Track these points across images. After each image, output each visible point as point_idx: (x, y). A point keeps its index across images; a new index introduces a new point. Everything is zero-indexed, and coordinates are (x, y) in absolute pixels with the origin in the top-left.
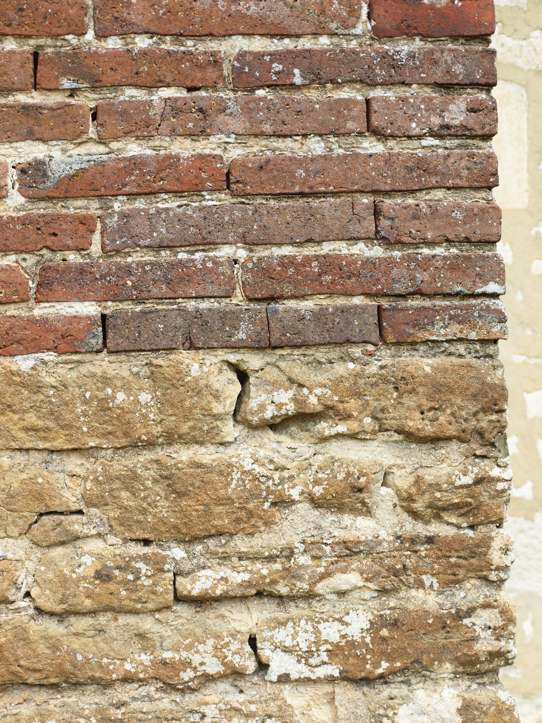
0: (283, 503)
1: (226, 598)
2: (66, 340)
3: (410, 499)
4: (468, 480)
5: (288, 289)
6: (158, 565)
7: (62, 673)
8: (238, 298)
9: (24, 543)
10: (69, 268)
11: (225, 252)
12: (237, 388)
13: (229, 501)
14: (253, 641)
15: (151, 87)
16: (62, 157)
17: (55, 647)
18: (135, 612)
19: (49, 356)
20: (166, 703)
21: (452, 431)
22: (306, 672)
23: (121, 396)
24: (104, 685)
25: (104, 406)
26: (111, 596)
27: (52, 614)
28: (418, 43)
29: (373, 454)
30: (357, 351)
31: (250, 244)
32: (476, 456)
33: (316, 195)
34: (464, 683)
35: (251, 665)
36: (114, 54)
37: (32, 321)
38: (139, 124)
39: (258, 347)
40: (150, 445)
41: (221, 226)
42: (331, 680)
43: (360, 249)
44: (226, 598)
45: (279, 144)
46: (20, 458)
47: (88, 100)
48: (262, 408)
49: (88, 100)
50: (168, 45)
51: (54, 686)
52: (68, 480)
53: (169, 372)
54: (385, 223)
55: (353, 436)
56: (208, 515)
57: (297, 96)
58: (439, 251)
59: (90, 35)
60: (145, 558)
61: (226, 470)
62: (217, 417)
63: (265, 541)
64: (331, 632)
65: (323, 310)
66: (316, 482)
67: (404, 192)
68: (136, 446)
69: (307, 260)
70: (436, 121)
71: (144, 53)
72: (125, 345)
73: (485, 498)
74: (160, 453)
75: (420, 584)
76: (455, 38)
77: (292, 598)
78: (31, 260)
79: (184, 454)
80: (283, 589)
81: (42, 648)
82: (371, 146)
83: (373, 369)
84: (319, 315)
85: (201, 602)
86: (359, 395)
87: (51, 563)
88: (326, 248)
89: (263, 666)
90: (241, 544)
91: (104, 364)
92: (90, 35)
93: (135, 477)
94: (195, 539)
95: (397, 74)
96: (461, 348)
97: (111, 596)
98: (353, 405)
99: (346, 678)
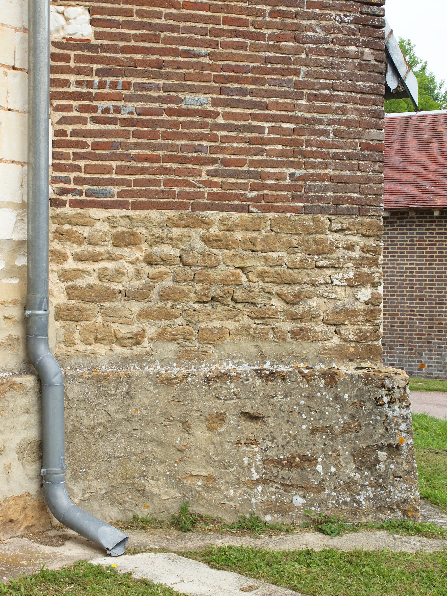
0: (338, 248)
1: (326, 267)
2: (296, 210)
3: (363, 248)
4: (375, 245)
5: (341, 203)
6: (312, 259)
7: (292, 281)
8: (331, 204)
9: (286, 253)
10: (298, 195)
11: (329, 194)
12: (329, 223)
13: (327, 246)
14: (330, 277)
15: (316, 158)
16: (298, 172)
17: (291, 275)
18: (307, 269)
19: (293, 214)
20: (312, 289)
21: (372, 234)
22: (341, 284)
23: (307, 223)
24: (300, 284)
25: (303, 225)
26: (303, 266)
27: (290, 268)
28: (369, 152)
29: (356, 239)
30: (354, 216)
31: (334, 192)
32: (320, 268)
33: (347, 183)
34: (372, 288)
35: (330, 282)
36: (309, 151)
37: (290, 206)
38: (313, 166)
39: (334, 215)
40: (312, 234)
41: (328, 188)
42: (345, 286)
43: (356, 195)
44: (326, 267)
45: (341, 172)
46: (286, 235)
47: (303, 160)
48: (334, 227)
49: (303, 160)
50: (319, 150)
51: (290, 284)
52: (295, 240)
53: (317, 218)
54: (361, 190)
55: (352, 235)
56: (323, 249)
57: (345, 162)
58: (371, 196)
59: (304, 147)
60: (310, 258)
61: (327, 240)
62: (326, 229)
63: (333, 255)
64: (346, 276)
65: (348, 207)
66: (345, 244)
67: (365, 184)
68: (309, 234)
69: (345, 197)
70: (372, 169)
71: (315, 151)
72: (308, 212)
73: (378, 249)
74: (314, 236)
75: (364, 267)
76: (376, 151)
77: (338, 268)
78: (290, 193)
79: (319, 236)
80: (337, 266)
81: (288, 275)
82: (359, 173)
83: (357, 220)
84: (347, 208)
85: (320, 268)
86: (354, 226)
87: (290, 258)
88: (349, 194)
89: (332, 282)
90: (329, 256)
91: (304, 216)
92: (304, 147)
93: (309, 240)
94: (320, 254)
95: (365, 158)
96: (375, 217)
97: (303, 266)
98: (353, 228)
99: (349, 286)
